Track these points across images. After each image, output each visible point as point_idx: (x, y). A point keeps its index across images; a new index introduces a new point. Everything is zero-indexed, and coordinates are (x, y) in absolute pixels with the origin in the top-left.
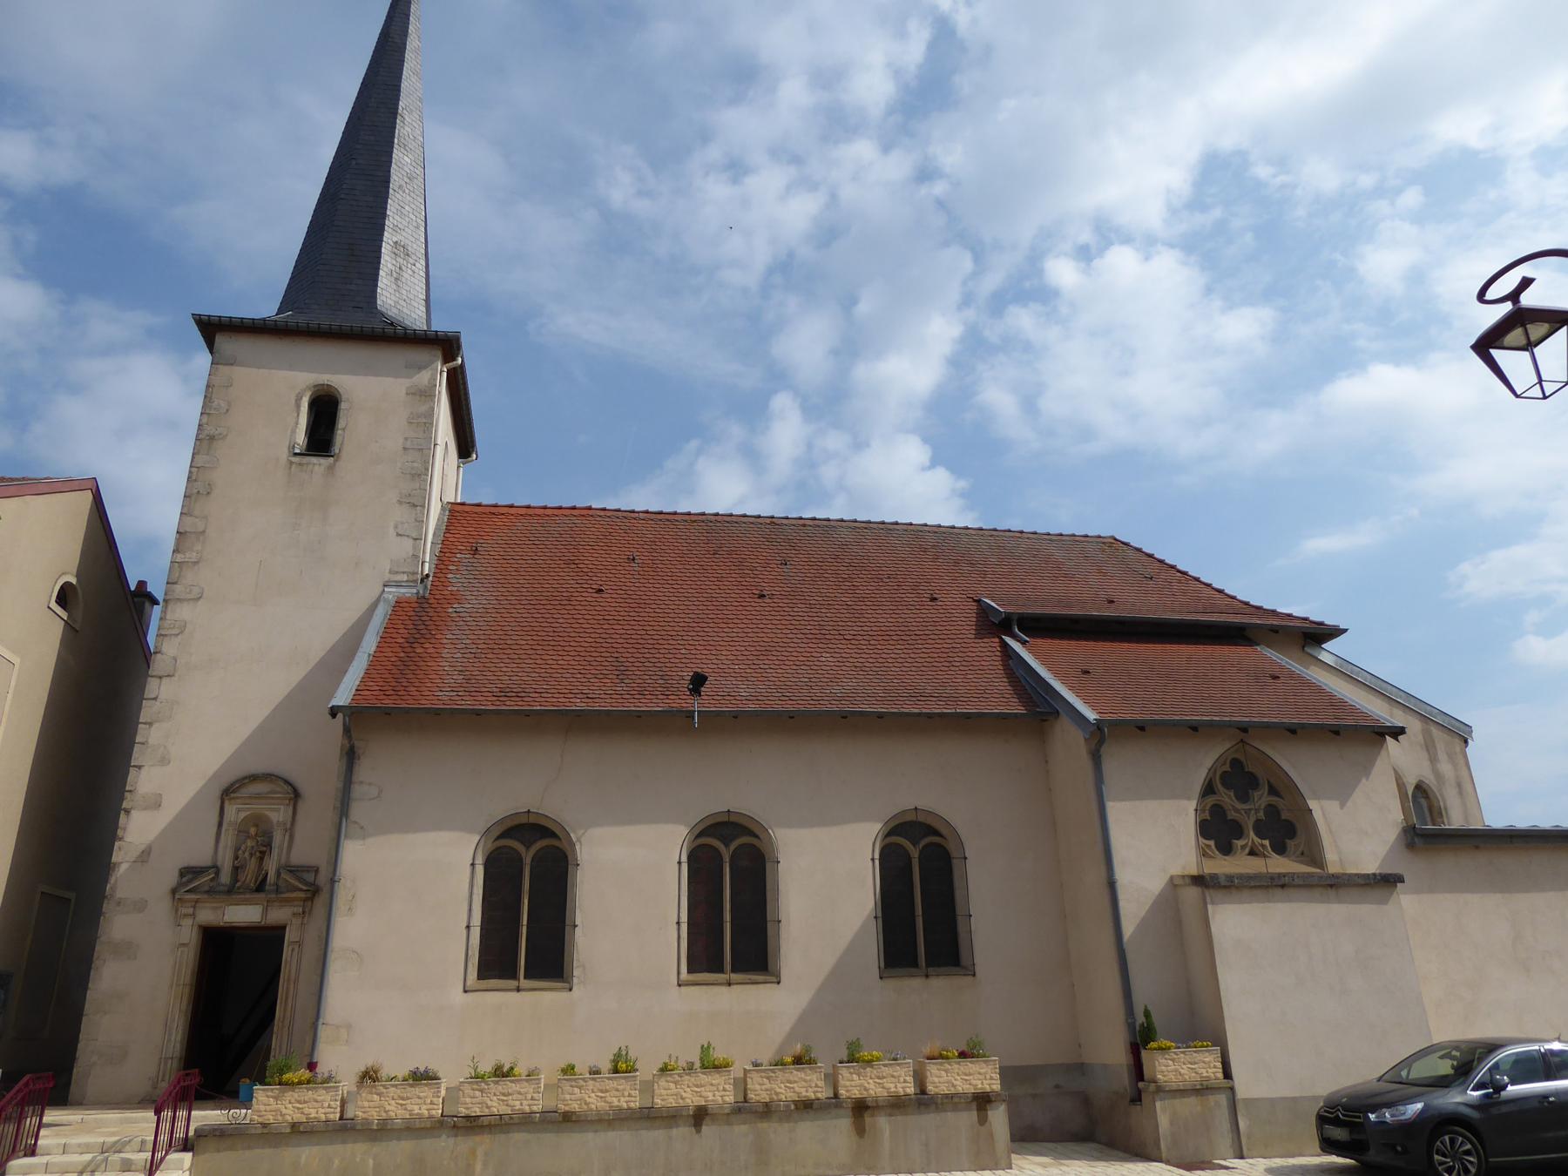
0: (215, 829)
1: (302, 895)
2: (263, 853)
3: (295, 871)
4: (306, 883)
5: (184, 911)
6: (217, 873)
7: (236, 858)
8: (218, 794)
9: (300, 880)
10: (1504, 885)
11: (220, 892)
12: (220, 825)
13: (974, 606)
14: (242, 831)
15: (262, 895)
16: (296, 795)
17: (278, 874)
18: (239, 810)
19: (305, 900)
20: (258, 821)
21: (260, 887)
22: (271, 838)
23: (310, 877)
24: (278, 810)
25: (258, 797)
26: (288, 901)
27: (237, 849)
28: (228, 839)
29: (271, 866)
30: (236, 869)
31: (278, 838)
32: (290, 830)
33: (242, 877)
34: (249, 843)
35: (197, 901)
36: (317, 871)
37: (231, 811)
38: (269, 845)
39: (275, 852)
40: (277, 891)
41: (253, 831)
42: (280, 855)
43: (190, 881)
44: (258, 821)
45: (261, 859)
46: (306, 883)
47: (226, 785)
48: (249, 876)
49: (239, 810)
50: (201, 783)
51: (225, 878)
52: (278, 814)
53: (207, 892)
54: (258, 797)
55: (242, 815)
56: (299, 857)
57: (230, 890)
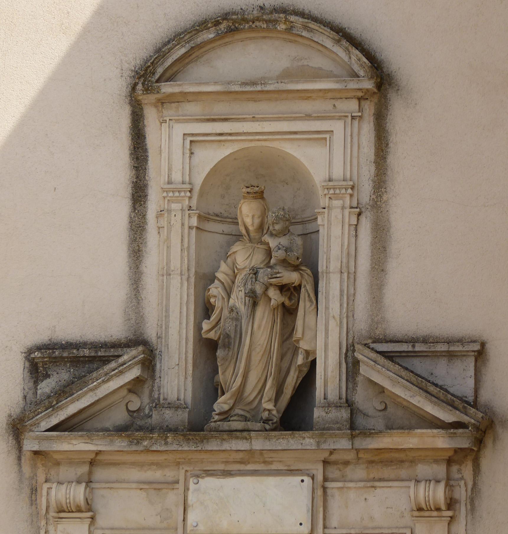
0: (122, 208)
1: (441, 441)
2: (290, 291)
3: (404, 353)
4: (452, 401)
5: (59, 494)
6: (149, 363)
7: (206, 310)
8: (117, 85)
9: (426, 385)
10: (308, 511)
11: (166, 430)
12: (139, 194)
13: (159, 219)
14: (212, 217)
15: (303, 441)
16: (380, 82)
17: (352, 367)
18: (194, 142)
19: (454, 458)
20: (259, 175)
21: (294, 415)
22: (310, 238)
23: (459, 377)
24: (322, 138)
25: (252, 91)
26: (390, 463)
27: (206, 279)
28: (171, 246)
29: (324, 336)
30: (209, 350)
31: (335, 238)
32: (374, 208)
33: (229, 376)
34: (244, 257)
35: (94, 461)
36: (481, 354)
37: (167, 138)
38: (307, 261)
39: (332, 286)
40: (354, 427)
41: (248, 213)
42: (349, 299)
43: (64, 392)
44: (259, 175)
45: (289, 312)
46: (452, 401)
47: (227, 9)
48: (252, 373)
49: (194, 142)
50: (59, 46)
51: (177, 379)
52: (326, 155)
53: (122, 430)
54: (252, 91)
55: (209, 158)
56: (408, 311)
57: (198, 426)
